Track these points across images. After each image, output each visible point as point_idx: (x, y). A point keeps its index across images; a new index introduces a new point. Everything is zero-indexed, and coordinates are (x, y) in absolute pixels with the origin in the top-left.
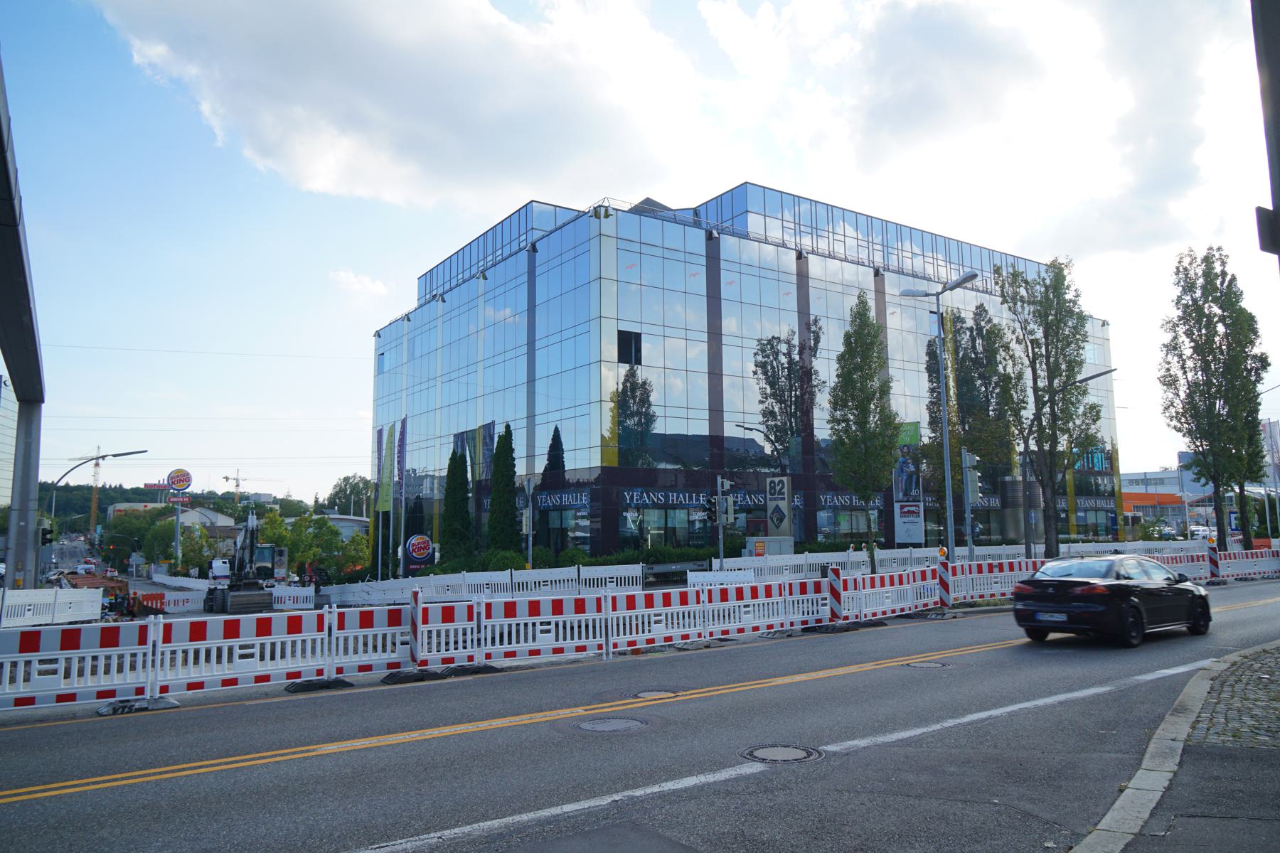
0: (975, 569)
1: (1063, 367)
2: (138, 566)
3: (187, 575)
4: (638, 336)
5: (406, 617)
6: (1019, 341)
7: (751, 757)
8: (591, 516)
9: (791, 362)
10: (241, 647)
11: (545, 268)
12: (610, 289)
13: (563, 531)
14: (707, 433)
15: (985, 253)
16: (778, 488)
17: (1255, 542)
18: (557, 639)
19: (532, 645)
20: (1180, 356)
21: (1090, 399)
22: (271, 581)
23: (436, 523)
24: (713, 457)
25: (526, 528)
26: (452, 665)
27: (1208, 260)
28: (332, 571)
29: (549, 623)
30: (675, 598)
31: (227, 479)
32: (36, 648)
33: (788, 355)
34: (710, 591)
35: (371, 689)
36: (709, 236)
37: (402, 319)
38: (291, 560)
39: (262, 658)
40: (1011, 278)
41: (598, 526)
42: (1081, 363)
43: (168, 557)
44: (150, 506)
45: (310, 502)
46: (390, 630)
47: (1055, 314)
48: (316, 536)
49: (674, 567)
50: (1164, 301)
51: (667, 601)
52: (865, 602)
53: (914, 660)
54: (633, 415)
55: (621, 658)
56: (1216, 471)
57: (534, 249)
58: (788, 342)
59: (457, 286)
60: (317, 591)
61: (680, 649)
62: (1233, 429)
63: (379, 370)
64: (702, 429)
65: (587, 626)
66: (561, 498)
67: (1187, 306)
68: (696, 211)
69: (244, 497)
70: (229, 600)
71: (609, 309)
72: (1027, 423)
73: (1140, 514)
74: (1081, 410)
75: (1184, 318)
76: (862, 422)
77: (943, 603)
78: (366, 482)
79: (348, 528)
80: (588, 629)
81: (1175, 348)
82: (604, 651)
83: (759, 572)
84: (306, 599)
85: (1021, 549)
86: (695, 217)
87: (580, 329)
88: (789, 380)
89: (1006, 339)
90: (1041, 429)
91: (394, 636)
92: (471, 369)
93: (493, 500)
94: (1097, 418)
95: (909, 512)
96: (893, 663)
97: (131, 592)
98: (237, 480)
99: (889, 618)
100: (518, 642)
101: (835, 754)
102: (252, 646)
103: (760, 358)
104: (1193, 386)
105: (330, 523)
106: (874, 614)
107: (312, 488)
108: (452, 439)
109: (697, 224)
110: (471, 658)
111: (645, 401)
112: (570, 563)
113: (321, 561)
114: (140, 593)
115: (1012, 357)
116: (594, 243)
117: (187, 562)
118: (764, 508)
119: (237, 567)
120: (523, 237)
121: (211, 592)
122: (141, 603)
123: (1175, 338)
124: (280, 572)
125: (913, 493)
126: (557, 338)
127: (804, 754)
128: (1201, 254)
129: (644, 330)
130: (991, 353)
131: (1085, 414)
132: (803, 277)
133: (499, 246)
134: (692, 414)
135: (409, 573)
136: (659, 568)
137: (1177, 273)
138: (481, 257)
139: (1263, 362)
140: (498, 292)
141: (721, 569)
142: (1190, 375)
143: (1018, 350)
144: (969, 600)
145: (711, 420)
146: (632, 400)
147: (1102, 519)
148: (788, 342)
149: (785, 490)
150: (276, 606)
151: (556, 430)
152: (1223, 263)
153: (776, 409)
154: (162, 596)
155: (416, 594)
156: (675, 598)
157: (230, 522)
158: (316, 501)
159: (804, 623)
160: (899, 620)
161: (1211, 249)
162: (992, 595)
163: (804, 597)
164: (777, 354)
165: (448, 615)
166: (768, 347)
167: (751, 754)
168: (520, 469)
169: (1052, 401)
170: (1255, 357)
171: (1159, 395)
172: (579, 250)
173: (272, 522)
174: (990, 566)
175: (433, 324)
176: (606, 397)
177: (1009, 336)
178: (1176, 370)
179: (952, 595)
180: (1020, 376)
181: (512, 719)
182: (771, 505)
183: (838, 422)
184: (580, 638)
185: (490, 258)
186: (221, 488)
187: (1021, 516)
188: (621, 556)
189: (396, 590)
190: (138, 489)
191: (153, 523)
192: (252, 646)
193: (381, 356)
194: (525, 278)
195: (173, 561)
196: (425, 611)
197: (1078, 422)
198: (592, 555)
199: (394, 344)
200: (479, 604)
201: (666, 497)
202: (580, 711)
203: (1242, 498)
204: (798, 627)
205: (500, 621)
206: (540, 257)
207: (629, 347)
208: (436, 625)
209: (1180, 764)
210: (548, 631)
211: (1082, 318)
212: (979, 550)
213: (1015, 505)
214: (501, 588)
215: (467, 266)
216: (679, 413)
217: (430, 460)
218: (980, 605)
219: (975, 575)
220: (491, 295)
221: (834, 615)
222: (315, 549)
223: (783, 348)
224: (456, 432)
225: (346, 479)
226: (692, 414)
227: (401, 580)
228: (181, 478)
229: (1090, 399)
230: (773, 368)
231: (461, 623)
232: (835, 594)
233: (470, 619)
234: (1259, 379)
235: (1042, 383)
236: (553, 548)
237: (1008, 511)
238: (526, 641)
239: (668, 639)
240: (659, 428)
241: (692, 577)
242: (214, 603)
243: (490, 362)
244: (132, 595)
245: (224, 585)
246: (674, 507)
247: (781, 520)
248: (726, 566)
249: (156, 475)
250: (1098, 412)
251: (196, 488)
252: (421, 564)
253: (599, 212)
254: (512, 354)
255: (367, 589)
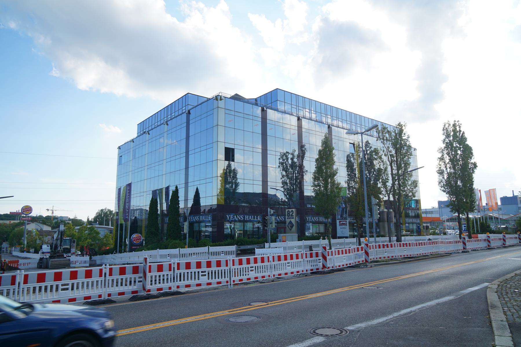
0: (377, 247)
1: (403, 165)
2: (6, 248)
3: (28, 252)
4: (233, 150)
5: (141, 270)
6: (385, 155)
7: (315, 334)
8: (212, 226)
9: (293, 162)
10: (62, 285)
11: (194, 120)
12: (221, 130)
13: (200, 232)
14: (261, 192)
15: (370, 121)
16: (291, 214)
17: (473, 235)
18: (209, 279)
19: (197, 282)
20: (445, 162)
21: (413, 179)
22: (70, 255)
23: (143, 229)
24: (262, 202)
25: (186, 230)
26: (161, 292)
27: (454, 125)
28: (97, 249)
29: (205, 272)
30: (252, 261)
31: (48, 210)
32: (60, 279)
33: (292, 159)
34: (273, 257)
35: (125, 304)
36: (263, 110)
37: (130, 141)
38: (78, 245)
39: (72, 289)
40: (380, 129)
41: (215, 230)
42: (409, 164)
43: (20, 244)
44: (12, 222)
45: (85, 220)
46: (133, 276)
47: (400, 146)
48: (89, 234)
49: (249, 247)
50: (438, 141)
51: (248, 262)
52: (336, 261)
53: (364, 285)
54: (229, 183)
55: (236, 287)
56: (459, 208)
57: (189, 113)
58: (292, 154)
59: (155, 128)
60: (90, 258)
61: (261, 282)
62: (465, 191)
63: (120, 163)
64: (258, 190)
65: (215, 273)
66: (199, 218)
67: (447, 143)
68: (256, 100)
69: (55, 218)
70: (50, 263)
71: (221, 138)
72: (389, 188)
73: (429, 225)
74: (410, 183)
75: (447, 147)
76: (326, 187)
77: (366, 261)
78: (111, 212)
79: (102, 231)
80: (223, 274)
81: (443, 159)
82: (229, 284)
83: (285, 248)
84: (85, 262)
85: (387, 239)
86: (255, 102)
87: (208, 147)
88: (293, 170)
89: (380, 154)
90: (394, 191)
91: (135, 278)
92: (161, 163)
93: (169, 218)
94: (416, 186)
95: (343, 224)
96: (356, 287)
97: (3, 260)
98: (53, 211)
99: (345, 268)
100: (212, 279)
101: (353, 331)
102: (68, 285)
103: (281, 160)
104: (449, 174)
105: (95, 229)
106: (339, 266)
107: (86, 213)
108: (151, 192)
109: (256, 104)
110: (170, 288)
111: (235, 177)
112: (204, 245)
113: (92, 245)
114: (7, 260)
115: (382, 161)
116: (215, 111)
117: (29, 246)
118: (285, 222)
119: (54, 248)
120: (184, 108)
121: (41, 259)
122: (7, 265)
123: (443, 155)
124: (73, 250)
125: (344, 216)
126: (199, 150)
127: (339, 332)
128: (452, 123)
129: (235, 147)
130: (371, 160)
131: (411, 184)
132: (300, 127)
133: (173, 111)
134: (255, 182)
135: (131, 250)
136: (243, 247)
137: (444, 130)
138: (166, 116)
139: (475, 165)
140: (173, 130)
141: (269, 248)
142: (448, 170)
143: (385, 158)
144: (375, 259)
145: (263, 185)
146: (229, 176)
147: (415, 227)
148: (292, 154)
149: (294, 214)
150: (71, 265)
151: (197, 189)
152: (460, 127)
153: (288, 182)
154: (18, 261)
155: (146, 259)
156: (252, 261)
157: (49, 229)
158: (88, 220)
159: (312, 270)
160: (349, 268)
161: (455, 121)
162: (384, 257)
163: (312, 259)
164: (287, 159)
165: (160, 268)
166: (284, 156)
167: (314, 332)
168: (182, 205)
169: (399, 179)
170: (472, 163)
171: (436, 177)
172: (209, 114)
173: (69, 228)
174: (383, 245)
175: (144, 144)
176: (219, 175)
177: (381, 153)
178: (443, 168)
179: (370, 257)
180: (386, 169)
181: (196, 317)
182: (288, 221)
183: (316, 186)
184: (218, 278)
185: (169, 116)
186: (45, 214)
187: (386, 226)
188: (226, 242)
189: (136, 257)
190: (7, 214)
191: (14, 229)
192: (68, 285)
193: (120, 157)
194: (185, 125)
195: (22, 246)
196: (150, 266)
197: (409, 188)
198: (213, 242)
199: (126, 152)
200: (174, 263)
201: (244, 217)
202: (226, 312)
203: (468, 219)
204: (309, 272)
205: (183, 270)
206: (191, 116)
207: (229, 154)
208: (155, 273)
209: (511, 332)
210: (205, 275)
211: (410, 147)
212: (378, 239)
213: (383, 221)
214: (175, 256)
215: (159, 119)
216: (249, 184)
217: (141, 202)
218: (380, 262)
219: (378, 249)
220: (170, 131)
221: (324, 267)
222: (88, 240)
223: (290, 156)
224: (153, 189)
225: (102, 210)
226: (255, 182)
227: (128, 253)
228: (27, 209)
229: (413, 179)
230: (286, 164)
231: (166, 272)
232: (325, 258)
233: (269, 262)
234: (473, 172)
235: (395, 172)
236: (197, 240)
237: (381, 223)
238: (215, 278)
239: (256, 278)
240: (241, 190)
241: (257, 251)
242: (42, 264)
243: (169, 160)
244: (3, 261)
245: (48, 256)
246: (247, 221)
247: (292, 227)
248: (271, 246)
249: (17, 208)
250: (417, 184)
251: (34, 214)
252: (137, 246)
253: (217, 98)
254: (178, 157)
255: (114, 257)
